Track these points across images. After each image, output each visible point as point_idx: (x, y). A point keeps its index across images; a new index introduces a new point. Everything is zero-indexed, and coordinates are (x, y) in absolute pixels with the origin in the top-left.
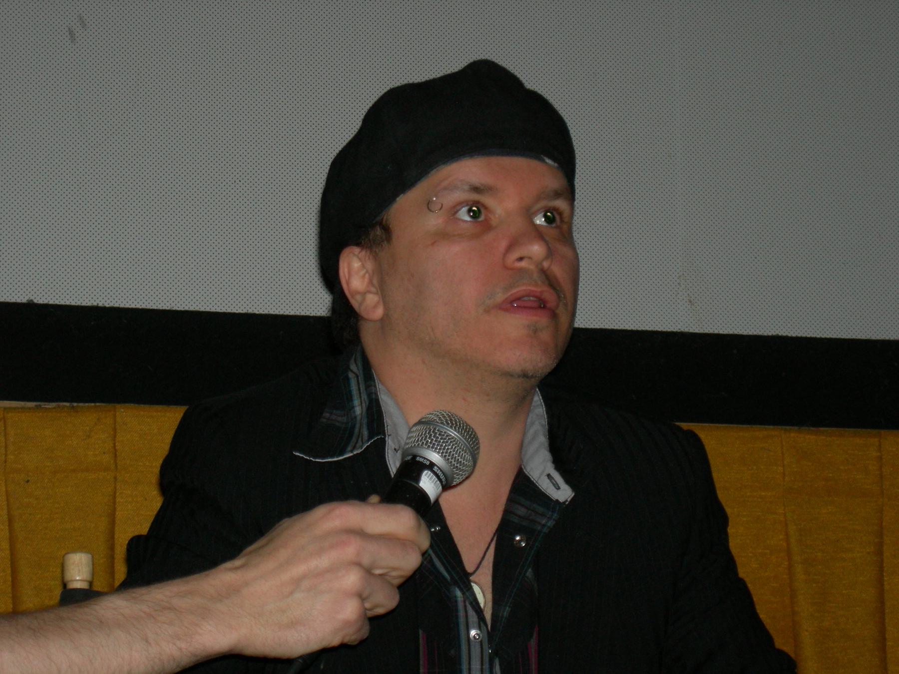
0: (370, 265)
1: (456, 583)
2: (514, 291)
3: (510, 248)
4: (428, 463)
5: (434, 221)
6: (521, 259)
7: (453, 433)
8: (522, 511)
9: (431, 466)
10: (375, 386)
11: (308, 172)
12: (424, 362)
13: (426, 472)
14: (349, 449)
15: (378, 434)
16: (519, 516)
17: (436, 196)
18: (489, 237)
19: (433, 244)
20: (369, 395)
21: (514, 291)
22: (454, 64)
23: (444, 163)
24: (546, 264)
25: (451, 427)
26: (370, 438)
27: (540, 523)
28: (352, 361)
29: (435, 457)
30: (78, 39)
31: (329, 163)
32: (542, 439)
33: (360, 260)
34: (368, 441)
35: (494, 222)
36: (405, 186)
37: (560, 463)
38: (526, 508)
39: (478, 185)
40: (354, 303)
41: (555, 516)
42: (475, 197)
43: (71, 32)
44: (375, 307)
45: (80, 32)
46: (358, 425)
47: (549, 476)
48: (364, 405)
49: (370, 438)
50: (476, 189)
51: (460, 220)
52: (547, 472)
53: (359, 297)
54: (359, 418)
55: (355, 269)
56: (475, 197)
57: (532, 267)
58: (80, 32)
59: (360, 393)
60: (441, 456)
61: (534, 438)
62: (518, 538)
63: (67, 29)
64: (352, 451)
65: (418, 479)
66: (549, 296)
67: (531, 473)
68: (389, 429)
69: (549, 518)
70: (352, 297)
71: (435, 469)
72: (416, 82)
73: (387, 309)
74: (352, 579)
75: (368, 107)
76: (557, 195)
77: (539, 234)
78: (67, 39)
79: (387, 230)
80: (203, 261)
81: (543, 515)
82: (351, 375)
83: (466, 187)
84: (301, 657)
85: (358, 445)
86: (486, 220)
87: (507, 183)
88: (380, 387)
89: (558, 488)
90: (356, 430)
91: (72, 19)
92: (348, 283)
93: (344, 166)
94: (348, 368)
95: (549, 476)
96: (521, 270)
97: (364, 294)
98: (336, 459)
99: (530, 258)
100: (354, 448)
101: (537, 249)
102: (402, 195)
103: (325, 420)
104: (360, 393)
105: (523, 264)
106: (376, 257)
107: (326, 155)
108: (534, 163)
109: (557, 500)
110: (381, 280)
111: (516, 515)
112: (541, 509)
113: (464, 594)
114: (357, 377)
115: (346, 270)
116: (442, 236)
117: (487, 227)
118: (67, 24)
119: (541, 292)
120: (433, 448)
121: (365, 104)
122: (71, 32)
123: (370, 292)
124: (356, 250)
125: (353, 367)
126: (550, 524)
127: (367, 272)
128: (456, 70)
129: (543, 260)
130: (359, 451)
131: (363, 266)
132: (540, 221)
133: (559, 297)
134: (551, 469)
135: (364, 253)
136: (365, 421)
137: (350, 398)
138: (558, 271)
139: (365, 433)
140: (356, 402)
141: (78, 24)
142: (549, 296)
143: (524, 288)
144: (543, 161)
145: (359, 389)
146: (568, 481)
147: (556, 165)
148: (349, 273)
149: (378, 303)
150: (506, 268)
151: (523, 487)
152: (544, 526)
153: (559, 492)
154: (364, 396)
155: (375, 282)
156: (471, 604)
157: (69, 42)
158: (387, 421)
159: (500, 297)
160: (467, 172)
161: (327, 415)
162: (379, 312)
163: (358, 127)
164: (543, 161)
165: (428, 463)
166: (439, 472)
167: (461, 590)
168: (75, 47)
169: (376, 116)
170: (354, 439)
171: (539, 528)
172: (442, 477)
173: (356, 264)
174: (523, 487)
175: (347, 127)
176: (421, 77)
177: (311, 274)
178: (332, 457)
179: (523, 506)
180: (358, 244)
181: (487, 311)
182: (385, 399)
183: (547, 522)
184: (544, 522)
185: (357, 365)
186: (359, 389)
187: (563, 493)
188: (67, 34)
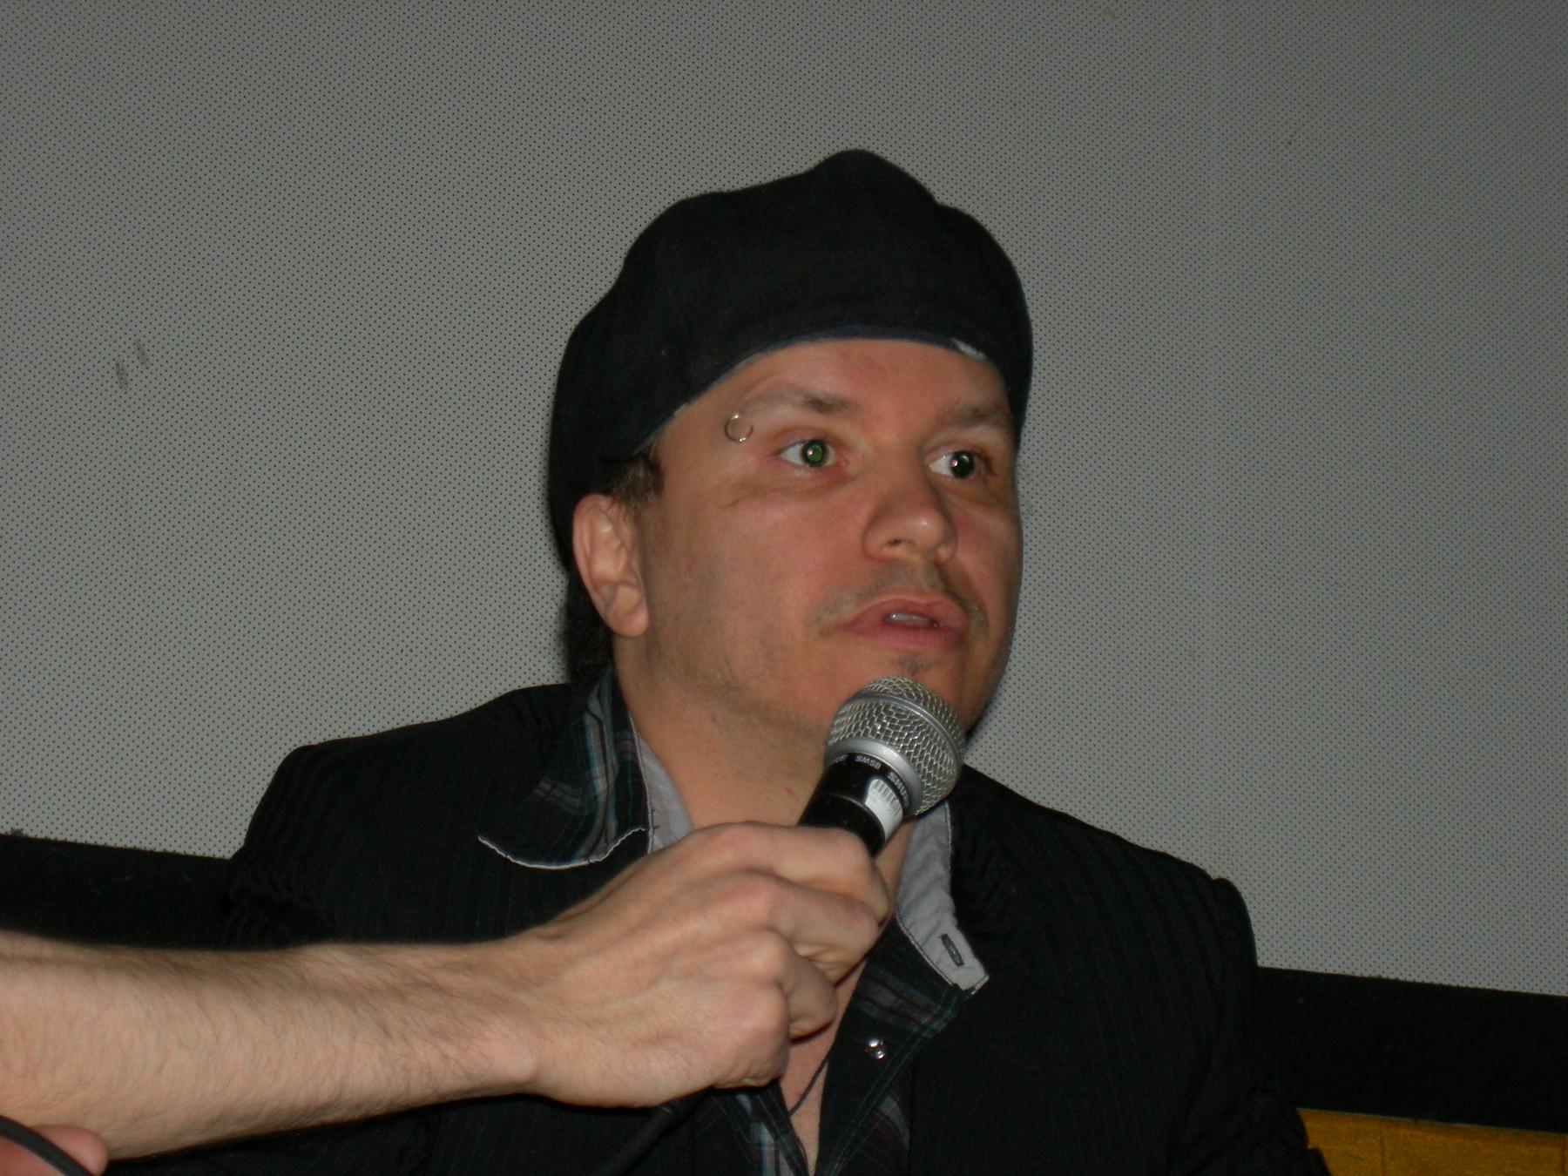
0: (627, 531)
1: (761, 1116)
2: (876, 601)
3: (876, 520)
4: (878, 766)
5: (739, 461)
6: (896, 542)
7: (919, 712)
8: (886, 998)
9: (884, 771)
10: (633, 740)
11: (367, 683)
12: (714, 719)
13: (874, 782)
14: (582, 851)
15: (634, 825)
16: (881, 1007)
17: (741, 413)
18: (840, 496)
19: (735, 503)
20: (621, 755)
21: (876, 601)
22: (800, 159)
23: (760, 350)
24: (944, 553)
25: (917, 702)
26: (620, 832)
27: (918, 1023)
28: (594, 695)
29: (888, 754)
30: (132, 384)
31: (567, 337)
32: (940, 870)
33: (610, 519)
34: (616, 839)
35: (851, 469)
36: (690, 388)
37: (966, 917)
38: (894, 992)
39: (822, 397)
40: (597, 599)
41: (949, 1013)
42: (818, 421)
43: (120, 371)
44: (633, 611)
45: (137, 371)
46: (601, 812)
47: (945, 938)
48: (611, 775)
49: (620, 832)
50: (819, 405)
51: (786, 462)
52: (942, 931)
53: (606, 590)
54: (602, 799)
55: (602, 534)
56: (818, 421)
57: (916, 558)
58: (137, 371)
59: (604, 754)
60: (902, 753)
61: (924, 866)
62: (874, 1044)
63: (113, 364)
64: (586, 857)
65: (861, 793)
66: (949, 612)
67: (912, 931)
68: (655, 817)
69: (937, 1017)
70: (596, 588)
71: (892, 776)
72: (725, 189)
73: (652, 616)
74: (764, 957)
75: (636, 234)
76: (978, 416)
77: (935, 496)
78: (112, 382)
79: (655, 468)
80: (279, 691)
81: (927, 1010)
82: (589, 720)
83: (799, 399)
84: (668, 1104)
85: (599, 847)
86: (837, 465)
87: (880, 390)
88: (640, 743)
89: (960, 963)
90: (598, 821)
91: (124, 347)
92: (589, 563)
93: (588, 343)
94: (585, 708)
95: (945, 938)
96: (893, 562)
97: (615, 585)
98: (554, 867)
99: (910, 542)
100: (592, 851)
101: (925, 526)
102: (683, 407)
103: (541, 794)
104: (604, 754)
105: (899, 551)
106: (638, 521)
107: (562, 324)
108: (936, 353)
109: (956, 986)
110: (647, 558)
111: (874, 1003)
112: (922, 999)
113: (776, 1137)
114: (600, 723)
115: (586, 538)
116: (751, 491)
117: (839, 478)
118: (114, 355)
119: (929, 606)
120: (887, 738)
121: (596, 289)
122: (120, 371)
123: (625, 583)
124: (603, 502)
125: (594, 705)
126: (939, 1026)
127: (623, 544)
128: (801, 171)
129: (939, 544)
130: (601, 858)
131: (616, 530)
132: (942, 465)
133: (966, 610)
134: (949, 926)
135: (615, 509)
136: (612, 802)
137: (587, 764)
138: (971, 561)
139: (613, 825)
140: (597, 769)
141: (134, 357)
142: (949, 612)
143: (893, 597)
144: (955, 348)
145: (603, 746)
146: (979, 953)
147: (981, 356)
148: (592, 543)
149: (638, 605)
150: (867, 555)
151: (892, 952)
152: (924, 1027)
153: (961, 971)
154: (612, 758)
155: (635, 565)
156: (788, 1158)
157: (116, 387)
158: (652, 802)
159: (849, 611)
160: (810, 367)
161: (545, 785)
162: (640, 621)
163: (616, 274)
164: (955, 348)
165: (878, 766)
166: (897, 782)
167: (772, 1130)
168: (146, 372)
169: (644, 256)
170: (592, 837)
171: (915, 1030)
172: (903, 793)
173: (605, 529)
174: (892, 952)
175: (598, 276)
176: (733, 182)
177: (532, 525)
178: (549, 861)
179: (888, 988)
180: (606, 492)
181: (825, 634)
182: (650, 767)
183: (932, 1022)
184: (925, 1020)
185: (601, 702)
186: (603, 746)
187: (968, 974)
188: (114, 372)
